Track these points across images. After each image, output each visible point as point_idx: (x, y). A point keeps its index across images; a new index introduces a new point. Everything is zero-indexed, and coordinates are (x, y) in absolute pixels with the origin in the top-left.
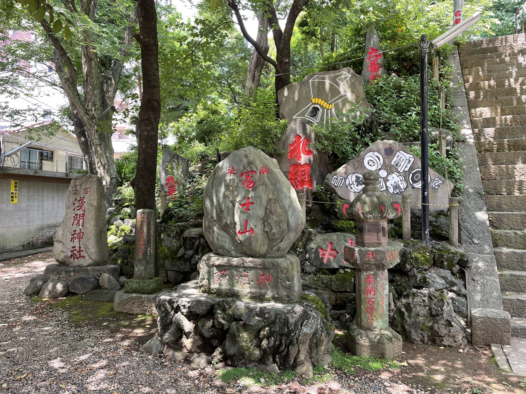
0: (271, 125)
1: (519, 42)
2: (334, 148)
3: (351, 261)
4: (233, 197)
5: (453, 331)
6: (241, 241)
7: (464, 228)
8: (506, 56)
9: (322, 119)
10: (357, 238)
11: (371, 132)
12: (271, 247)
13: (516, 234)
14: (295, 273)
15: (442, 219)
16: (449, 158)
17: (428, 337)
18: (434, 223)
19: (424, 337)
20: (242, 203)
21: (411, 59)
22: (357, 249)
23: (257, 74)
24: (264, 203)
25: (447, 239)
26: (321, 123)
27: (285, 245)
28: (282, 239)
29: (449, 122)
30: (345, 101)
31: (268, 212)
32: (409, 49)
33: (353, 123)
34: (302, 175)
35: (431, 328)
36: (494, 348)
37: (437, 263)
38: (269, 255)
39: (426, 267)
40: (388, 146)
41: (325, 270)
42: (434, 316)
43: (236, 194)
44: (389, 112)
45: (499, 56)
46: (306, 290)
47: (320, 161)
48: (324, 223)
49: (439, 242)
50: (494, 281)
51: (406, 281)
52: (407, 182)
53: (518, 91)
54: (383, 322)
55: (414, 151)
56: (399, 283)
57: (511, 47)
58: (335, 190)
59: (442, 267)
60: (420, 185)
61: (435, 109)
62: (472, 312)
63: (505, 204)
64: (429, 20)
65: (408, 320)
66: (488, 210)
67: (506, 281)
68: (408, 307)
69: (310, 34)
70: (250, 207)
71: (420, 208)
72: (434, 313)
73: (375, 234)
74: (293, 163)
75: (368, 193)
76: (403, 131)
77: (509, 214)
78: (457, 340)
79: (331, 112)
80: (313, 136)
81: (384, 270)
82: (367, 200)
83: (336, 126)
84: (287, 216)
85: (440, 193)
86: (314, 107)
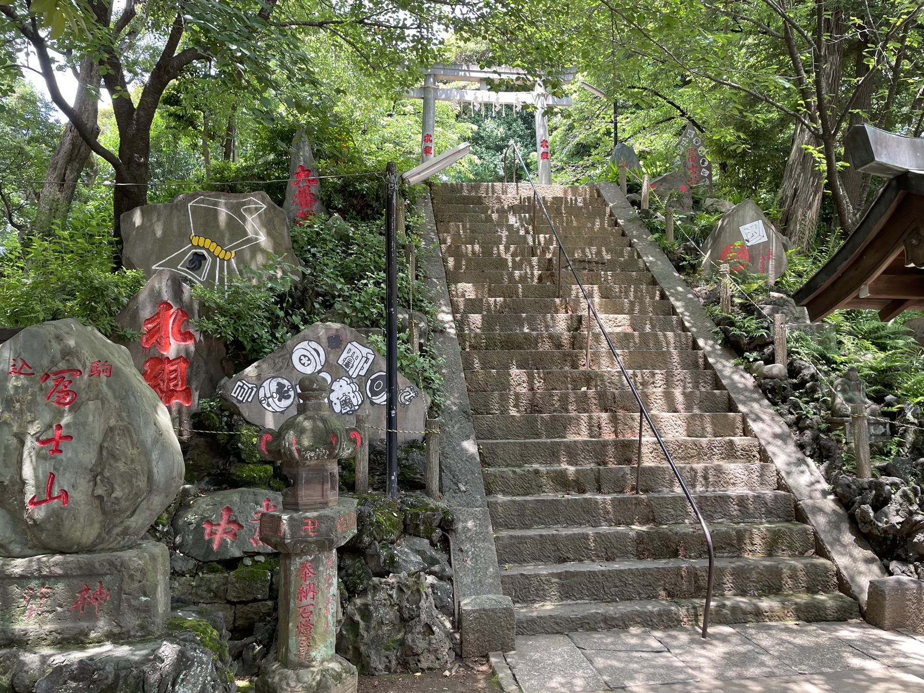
0: (105, 278)
1: (509, 195)
2: (237, 330)
3: (273, 541)
4: (20, 426)
5: (434, 641)
6: (35, 521)
7: (446, 467)
8: (493, 212)
9: (211, 275)
10: (284, 495)
11: (303, 306)
12: (107, 528)
13: (514, 472)
14: (160, 577)
15: (416, 454)
16: (424, 356)
17: (397, 659)
18: (404, 462)
19: (390, 662)
20: (43, 438)
21: (363, 196)
22: (285, 517)
23: (70, 176)
24: (98, 436)
25: (421, 486)
26: (209, 283)
27: (139, 521)
28: (134, 511)
29: (422, 301)
30: (256, 249)
31: (106, 454)
32: (361, 179)
33: (271, 289)
34: (170, 380)
35: (402, 643)
36: (493, 660)
37: (409, 528)
38: (101, 546)
39: (393, 537)
40: (334, 332)
41: (215, 564)
42: (405, 620)
43: (29, 419)
44: (331, 276)
45: (485, 210)
46: (178, 608)
47: (209, 354)
48: (214, 471)
49: (411, 493)
50: (489, 549)
51: (362, 565)
52: (362, 391)
53: (510, 264)
54: (326, 647)
55: (373, 342)
56: (350, 571)
57: (499, 199)
58: (237, 408)
59: (417, 535)
60: (385, 398)
61: (402, 279)
62: (462, 604)
63: (499, 428)
64: (385, 140)
65: (365, 634)
66: (478, 438)
67: (505, 547)
68: (365, 612)
69: (184, 122)
70: (63, 445)
71: (384, 437)
72: (406, 616)
73: (319, 487)
74: (151, 355)
75: (309, 413)
76: (355, 309)
77: (504, 443)
78: (440, 656)
79: (228, 266)
80: (196, 307)
81: (331, 550)
82: (307, 424)
83: (241, 291)
84: (149, 462)
85: (411, 413)
86: (196, 253)
